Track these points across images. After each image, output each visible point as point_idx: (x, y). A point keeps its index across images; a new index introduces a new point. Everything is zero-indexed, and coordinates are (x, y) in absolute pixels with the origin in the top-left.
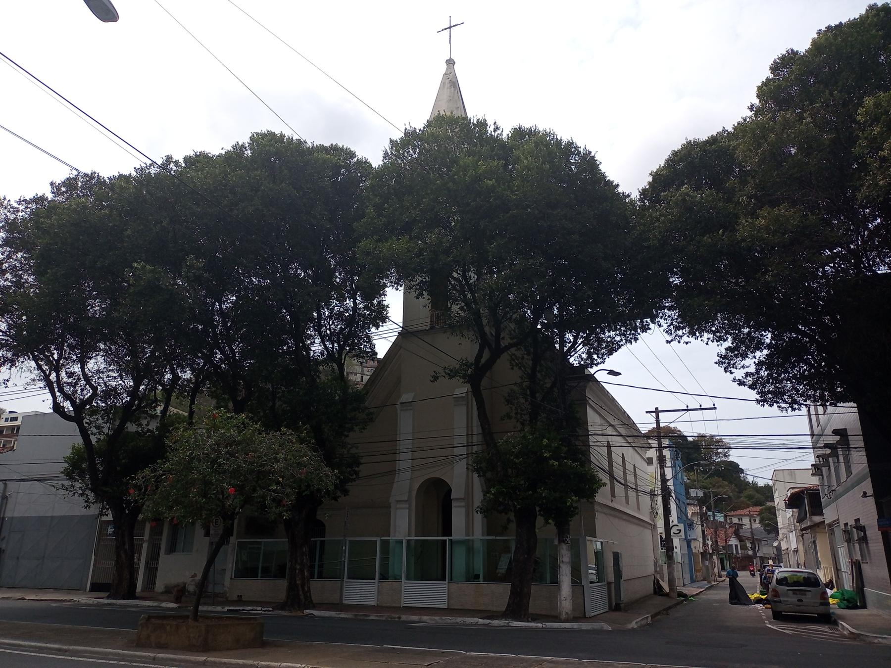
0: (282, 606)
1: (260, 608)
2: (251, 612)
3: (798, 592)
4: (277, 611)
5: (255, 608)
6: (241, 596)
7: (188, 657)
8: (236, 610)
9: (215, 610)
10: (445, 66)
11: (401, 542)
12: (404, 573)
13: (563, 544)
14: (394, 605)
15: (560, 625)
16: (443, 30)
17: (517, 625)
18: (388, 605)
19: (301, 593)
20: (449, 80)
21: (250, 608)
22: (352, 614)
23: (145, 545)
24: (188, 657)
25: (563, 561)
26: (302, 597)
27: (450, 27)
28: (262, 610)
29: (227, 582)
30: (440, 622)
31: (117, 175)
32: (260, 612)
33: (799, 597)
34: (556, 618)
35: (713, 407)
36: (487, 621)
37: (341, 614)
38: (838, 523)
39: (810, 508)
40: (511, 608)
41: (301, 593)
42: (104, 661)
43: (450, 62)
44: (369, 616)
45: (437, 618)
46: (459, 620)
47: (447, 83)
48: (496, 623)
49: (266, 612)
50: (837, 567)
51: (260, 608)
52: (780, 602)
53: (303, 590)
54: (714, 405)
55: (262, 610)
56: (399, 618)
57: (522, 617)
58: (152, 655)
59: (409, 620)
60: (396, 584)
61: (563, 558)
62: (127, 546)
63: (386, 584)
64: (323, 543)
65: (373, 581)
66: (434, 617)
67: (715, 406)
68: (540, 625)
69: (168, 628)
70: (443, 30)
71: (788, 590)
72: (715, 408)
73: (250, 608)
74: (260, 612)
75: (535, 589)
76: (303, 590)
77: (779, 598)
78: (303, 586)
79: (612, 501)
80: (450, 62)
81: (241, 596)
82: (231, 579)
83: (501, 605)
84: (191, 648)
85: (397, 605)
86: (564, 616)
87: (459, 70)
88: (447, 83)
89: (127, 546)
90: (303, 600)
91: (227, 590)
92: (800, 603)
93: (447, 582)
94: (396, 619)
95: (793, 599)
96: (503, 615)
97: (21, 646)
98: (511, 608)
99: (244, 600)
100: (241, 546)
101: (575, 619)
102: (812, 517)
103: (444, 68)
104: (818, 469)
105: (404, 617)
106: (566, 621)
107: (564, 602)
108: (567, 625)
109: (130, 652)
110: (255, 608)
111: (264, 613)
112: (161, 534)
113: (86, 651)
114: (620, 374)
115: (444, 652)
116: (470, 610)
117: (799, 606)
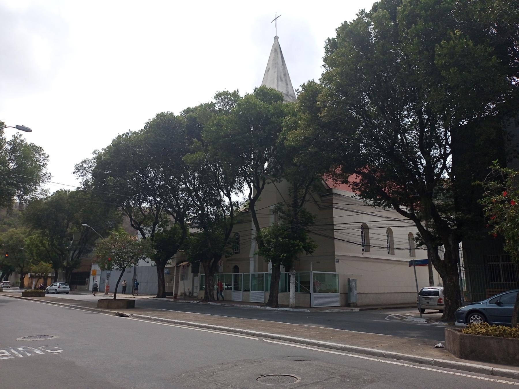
3: (427, 299)
10: (274, 40)
19: (209, 295)
23: (175, 277)
26: (209, 297)
30: (246, 307)
31: (222, 92)
33: (428, 301)
34: (287, 306)
36: (259, 307)
41: (209, 295)
43: (276, 38)
45: (245, 306)
46: (251, 306)
48: (262, 308)
53: (210, 294)
56: (234, 305)
62: (161, 277)
63: (246, 292)
76: (210, 294)
78: (210, 292)
79: (363, 254)
80: (276, 38)
85: (248, 301)
89: (161, 277)
92: (427, 304)
93: (242, 291)
101: (296, 307)
103: (273, 40)
106: (291, 308)
108: (291, 309)
112: (179, 273)
115: (334, 331)
117: (427, 305)
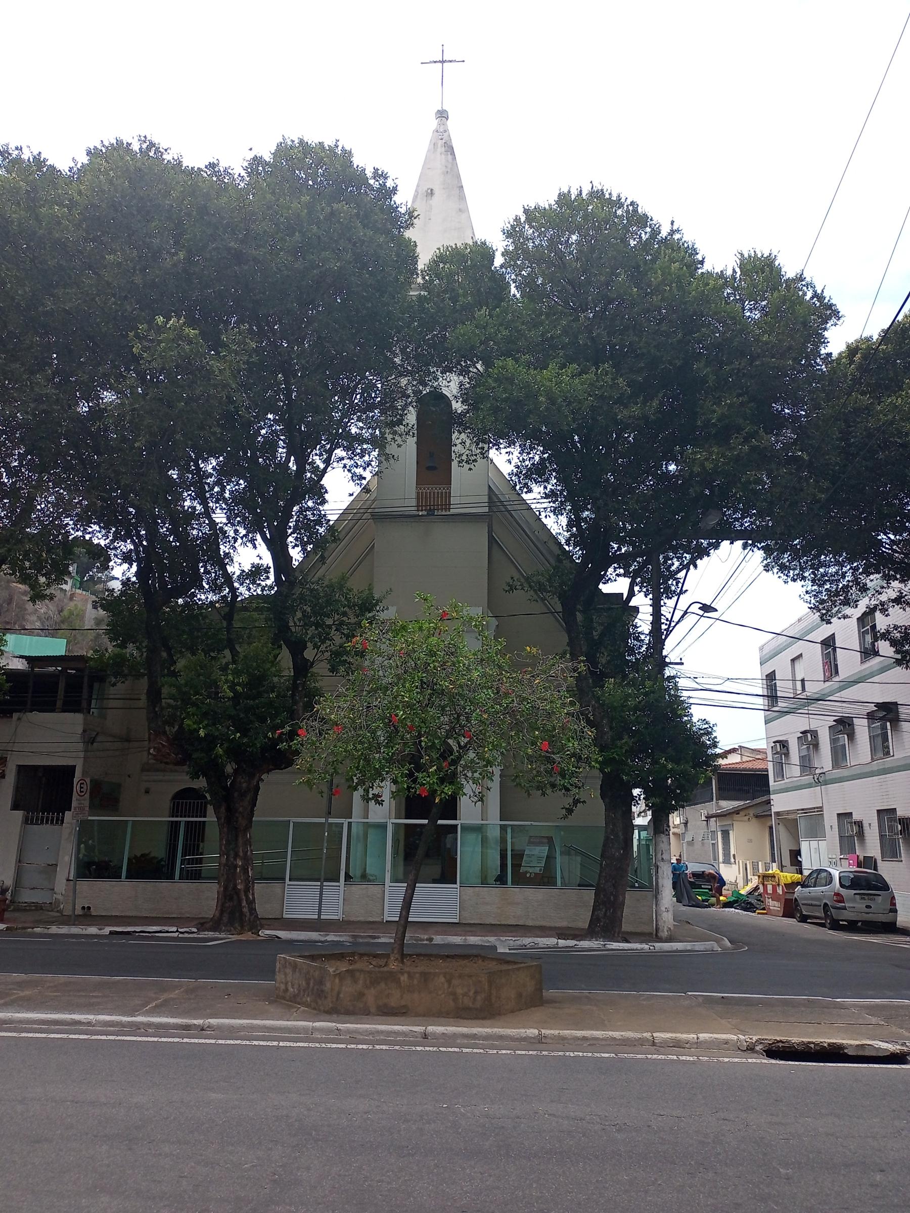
0: (215, 925)
1: (174, 929)
2: (157, 934)
3: (866, 897)
4: (206, 933)
5: (166, 928)
6: (89, 908)
7: (475, 1030)
8: (128, 933)
9: (84, 932)
11: (383, 827)
12: (388, 871)
13: (662, 835)
14: (371, 919)
15: (671, 945)
16: (430, 62)
17: (618, 948)
18: (362, 919)
19: (244, 903)
20: (444, 141)
21: (155, 928)
22: (349, 935)
24: (475, 1030)
25: (663, 859)
26: (245, 910)
27: (443, 62)
28: (177, 931)
29: (61, 885)
32: (176, 935)
35: (680, 661)
37: (328, 935)
38: (822, 811)
39: (717, 791)
40: (602, 924)
42: (306, 1045)
44: (378, 937)
46: (527, 941)
47: (439, 145)
49: (186, 935)
50: (781, 863)
51: (174, 929)
52: (844, 908)
54: (681, 659)
55: (177, 931)
56: (431, 940)
57: (616, 935)
58: (419, 1029)
59: (446, 942)
60: (374, 890)
61: (664, 855)
63: (358, 890)
64: (350, 824)
65: (337, 884)
66: (487, 938)
67: (682, 661)
68: (645, 946)
69: (404, 978)
70: (430, 62)
71: (855, 894)
72: (682, 664)
73: (155, 928)
74: (176, 935)
75: (630, 898)
77: (844, 905)
78: (247, 890)
80: (442, 115)
81: (89, 908)
82: (68, 880)
83: (583, 920)
84: (462, 1013)
86: (664, 934)
87: (455, 129)
88: (439, 145)
90: (248, 914)
91: (59, 897)
94: (425, 942)
95: (861, 905)
96: (590, 932)
97: (79, 1023)
98: (602, 924)
99: (94, 914)
100: (85, 828)
102: (720, 801)
103: (434, 123)
104: (784, 746)
105: (438, 939)
107: (665, 914)
109: (486, 1030)
110: (166, 928)
111: (181, 935)
113: (253, 1028)
114: (717, 610)
116: (494, 925)
